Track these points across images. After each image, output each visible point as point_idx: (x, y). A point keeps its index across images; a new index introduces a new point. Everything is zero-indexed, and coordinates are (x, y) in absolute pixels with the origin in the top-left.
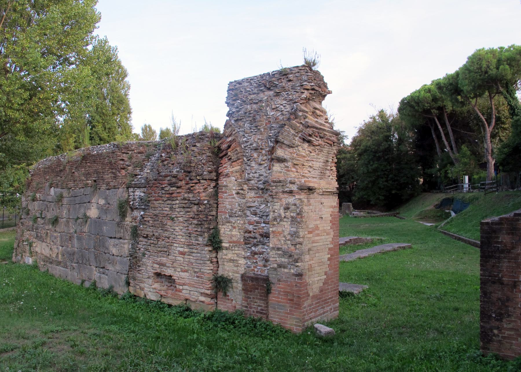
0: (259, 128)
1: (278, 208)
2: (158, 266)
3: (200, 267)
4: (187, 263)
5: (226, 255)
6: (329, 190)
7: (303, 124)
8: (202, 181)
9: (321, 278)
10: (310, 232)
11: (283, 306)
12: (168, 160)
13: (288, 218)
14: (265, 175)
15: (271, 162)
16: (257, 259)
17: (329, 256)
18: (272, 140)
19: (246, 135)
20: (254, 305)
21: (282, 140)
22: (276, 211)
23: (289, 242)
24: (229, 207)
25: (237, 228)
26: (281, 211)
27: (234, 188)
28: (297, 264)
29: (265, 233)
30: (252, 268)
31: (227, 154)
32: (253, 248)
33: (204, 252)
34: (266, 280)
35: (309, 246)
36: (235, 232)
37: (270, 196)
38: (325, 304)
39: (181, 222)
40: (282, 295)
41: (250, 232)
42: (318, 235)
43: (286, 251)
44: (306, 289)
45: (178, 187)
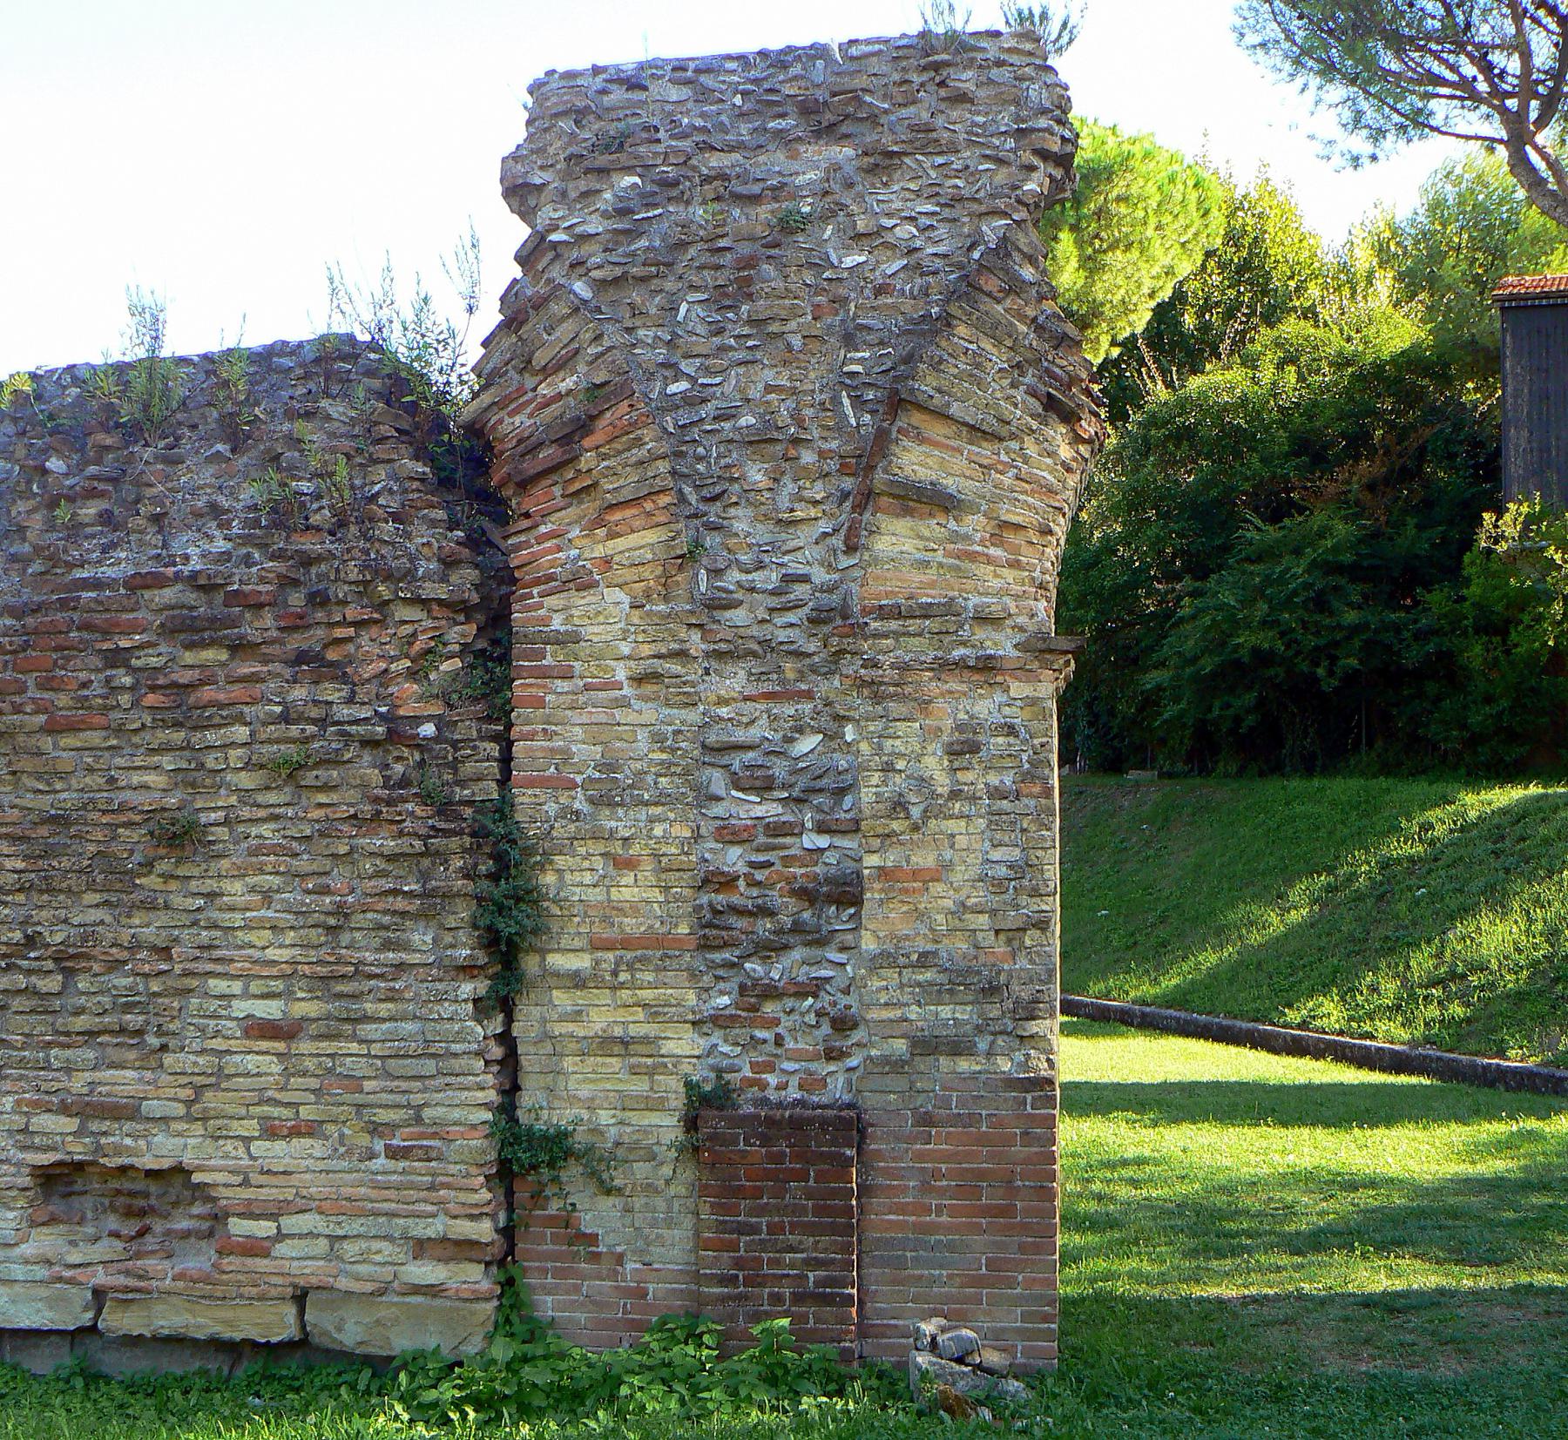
0: (774, 327)
2: (71, 1124)
3: (417, 1099)
4: (314, 1083)
5: (577, 1016)
8: (403, 612)
12: (102, 495)
13: (974, 799)
14: (820, 575)
15: (859, 508)
16: (777, 1022)
19: (687, 367)
20: (775, 1263)
21: (938, 400)
22: (901, 765)
23: (983, 920)
24: (586, 752)
25: (648, 865)
27: (625, 649)
29: (828, 880)
33: (447, 1009)
36: (628, 890)
37: (861, 683)
39: (275, 850)
40: (942, 1192)
41: (728, 882)
43: (963, 964)
45: (239, 648)
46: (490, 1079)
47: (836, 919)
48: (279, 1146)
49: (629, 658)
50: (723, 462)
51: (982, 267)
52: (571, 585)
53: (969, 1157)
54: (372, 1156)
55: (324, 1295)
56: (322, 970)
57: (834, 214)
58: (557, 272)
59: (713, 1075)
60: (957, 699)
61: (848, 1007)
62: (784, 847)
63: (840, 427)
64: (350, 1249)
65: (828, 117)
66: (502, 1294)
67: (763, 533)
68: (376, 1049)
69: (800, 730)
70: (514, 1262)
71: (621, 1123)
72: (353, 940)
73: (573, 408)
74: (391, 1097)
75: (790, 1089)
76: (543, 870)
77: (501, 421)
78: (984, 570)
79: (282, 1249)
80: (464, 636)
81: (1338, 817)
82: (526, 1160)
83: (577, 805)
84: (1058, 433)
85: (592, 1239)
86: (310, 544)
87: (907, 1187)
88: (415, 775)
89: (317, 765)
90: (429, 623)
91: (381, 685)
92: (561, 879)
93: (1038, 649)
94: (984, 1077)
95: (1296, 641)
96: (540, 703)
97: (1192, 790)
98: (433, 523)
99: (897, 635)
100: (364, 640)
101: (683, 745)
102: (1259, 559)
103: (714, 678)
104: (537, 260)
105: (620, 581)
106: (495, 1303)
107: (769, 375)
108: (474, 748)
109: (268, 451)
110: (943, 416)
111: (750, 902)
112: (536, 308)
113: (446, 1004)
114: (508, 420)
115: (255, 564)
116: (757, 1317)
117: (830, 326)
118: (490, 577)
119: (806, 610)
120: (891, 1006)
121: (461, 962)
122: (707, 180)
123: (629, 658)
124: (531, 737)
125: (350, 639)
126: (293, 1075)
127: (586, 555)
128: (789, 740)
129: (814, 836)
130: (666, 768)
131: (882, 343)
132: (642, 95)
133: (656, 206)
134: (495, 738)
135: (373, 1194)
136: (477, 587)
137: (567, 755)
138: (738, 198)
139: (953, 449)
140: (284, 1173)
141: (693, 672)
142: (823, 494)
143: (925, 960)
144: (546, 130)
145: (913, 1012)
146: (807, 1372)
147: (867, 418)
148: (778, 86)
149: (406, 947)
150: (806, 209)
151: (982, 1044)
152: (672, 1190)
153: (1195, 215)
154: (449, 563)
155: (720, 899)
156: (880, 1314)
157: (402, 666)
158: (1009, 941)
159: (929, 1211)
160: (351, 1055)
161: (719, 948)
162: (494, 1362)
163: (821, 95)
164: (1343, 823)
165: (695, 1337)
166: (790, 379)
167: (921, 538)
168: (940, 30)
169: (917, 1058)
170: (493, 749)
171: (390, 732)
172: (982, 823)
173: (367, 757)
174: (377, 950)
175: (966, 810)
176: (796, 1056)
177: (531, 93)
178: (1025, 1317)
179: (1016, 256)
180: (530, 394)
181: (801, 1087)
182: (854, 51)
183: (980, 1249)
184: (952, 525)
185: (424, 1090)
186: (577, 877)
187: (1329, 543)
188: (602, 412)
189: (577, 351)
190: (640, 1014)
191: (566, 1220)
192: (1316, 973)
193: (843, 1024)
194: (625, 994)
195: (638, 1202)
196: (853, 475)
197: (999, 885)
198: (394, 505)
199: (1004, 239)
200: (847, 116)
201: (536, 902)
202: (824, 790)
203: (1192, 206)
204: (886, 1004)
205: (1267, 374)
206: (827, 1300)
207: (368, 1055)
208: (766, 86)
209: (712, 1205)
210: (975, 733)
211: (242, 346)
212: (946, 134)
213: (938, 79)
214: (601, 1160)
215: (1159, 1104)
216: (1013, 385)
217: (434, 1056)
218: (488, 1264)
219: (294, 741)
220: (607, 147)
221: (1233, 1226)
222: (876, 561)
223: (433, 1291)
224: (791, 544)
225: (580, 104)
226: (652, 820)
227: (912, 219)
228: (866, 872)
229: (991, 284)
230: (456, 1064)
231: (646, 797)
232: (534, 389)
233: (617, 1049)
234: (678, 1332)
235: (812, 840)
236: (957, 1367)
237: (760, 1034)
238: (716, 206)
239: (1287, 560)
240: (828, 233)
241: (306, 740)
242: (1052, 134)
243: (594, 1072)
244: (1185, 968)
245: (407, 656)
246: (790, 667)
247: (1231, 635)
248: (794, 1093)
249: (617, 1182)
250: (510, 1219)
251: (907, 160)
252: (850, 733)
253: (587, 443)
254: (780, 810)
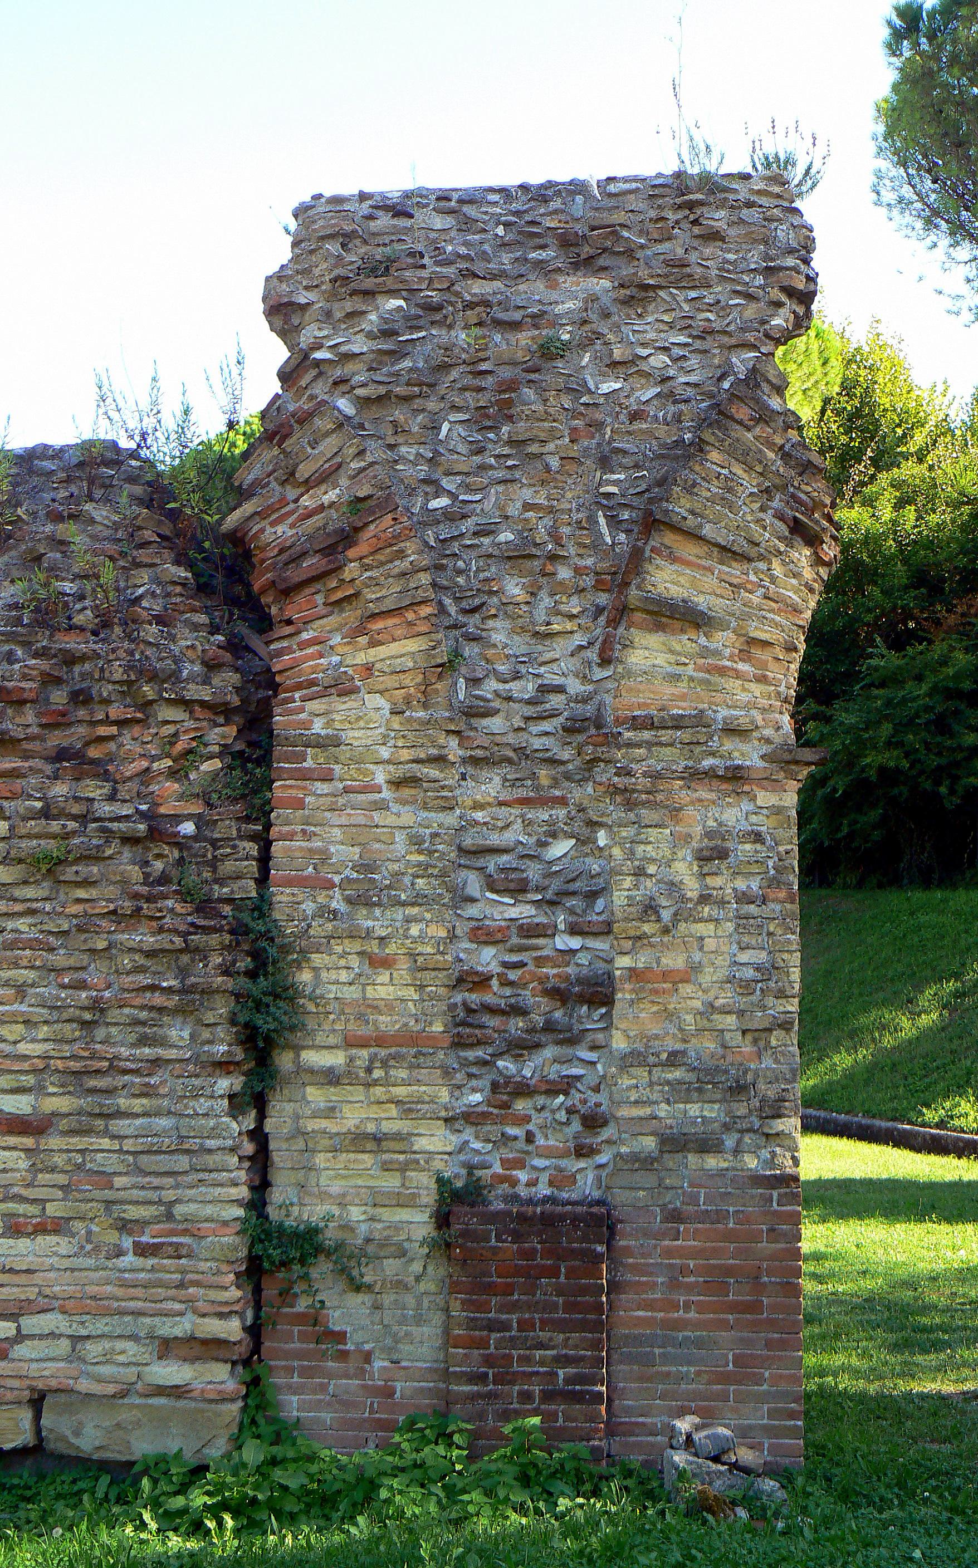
0: (534, 448)
3: (169, 1195)
4: (62, 1179)
5: (330, 1112)
11: (699, 1344)
13: (722, 903)
14: (575, 686)
15: (614, 622)
16: (527, 1119)
19: (448, 483)
21: (691, 522)
22: (651, 869)
23: (731, 1020)
24: (344, 854)
25: (404, 964)
26: (680, 867)
27: (385, 753)
29: (580, 981)
30: (498, 1168)
32: (506, 1064)
33: (203, 1105)
36: (384, 988)
37: (614, 791)
39: (32, 945)
40: (690, 1288)
41: (482, 982)
43: (711, 1063)
46: (242, 1175)
47: (587, 1017)
48: (23, 1244)
49: (388, 762)
50: (482, 576)
51: (733, 397)
52: (333, 690)
53: (715, 1253)
54: (120, 1253)
55: (62, 1398)
56: (74, 1065)
57: (591, 342)
58: (320, 390)
59: (464, 1172)
60: (706, 807)
61: (598, 1105)
62: (537, 948)
63: (596, 546)
64: (93, 1349)
65: (586, 250)
66: (246, 1396)
67: (519, 645)
68: (128, 1145)
69: (554, 835)
70: (260, 1360)
71: (372, 1219)
72: (109, 1035)
73: (336, 520)
74: (142, 1193)
75: (540, 1185)
76: (299, 968)
77: (262, 530)
78: (733, 684)
79: (21, 1350)
80: (224, 737)
81: (962, 927)
82: (276, 1257)
83: (334, 905)
84: (802, 555)
85: (341, 1337)
86: (72, 643)
87: (655, 1284)
88: (175, 873)
89: (77, 861)
90: (191, 724)
91: (142, 783)
92: (317, 977)
93: (782, 760)
94: (730, 1174)
95: (919, 761)
96: (299, 804)
97: (820, 900)
98: (196, 627)
99: (649, 745)
100: (126, 739)
101: (440, 847)
102: (882, 685)
103: (470, 783)
104: (300, 377)
105: (381, 687)
106: (240, 1404)
107: (527, 494)
108: (234, 847)
109: (31, 550)
110: (697, 537)
111: (503, 1001)
112: (301, 422)
113: (202, 1100)
114: (269, 530)
115: (18, 661)
116: (506, 1416)
117: (587, 449)
118: (248, 681)
119: (562, 719)
120: (642, 1105)
121: (218, 1058)
122: (470, 306)
123: (388, 762)
124: (290, 837)
125: (112, 738)
126: (41, 1171)
127: (348, 662)
128: (543, 844)
129: (566, 938)
130: (423, 870)
131: (637, 466)
132: (407, 223)
133: (419, 328)
134: (253, 838)
135: (120, 1292)
136: (238, 690)
137: (325, 856)
138: (498, 323)
139: (705, 568)
140: (28, 1271)
141: (450, 777)
142: (579, 609)
143: (675, 1059)
144: (312, 252)
145: (663, 1110)
146: (559, 1472)
147: (622, 537)
148: (538, 219)
149: (162, 1042)
150: (566, 337)
151: (730, 1142)
152: (422, 1287)
153: (818, 363)
154: (211, 666)
155: (474, 998)
156: (628, 1411)
157: (163, 764)
158: (755, 1041)
159: (676, 1307)
160: (103, 1151)
161: (471, 1046)
162: (244, 1465)
163: (580, 228)
164: (966, 932)
165: (445, 1437)
166: (548, 498)
167: (672, 652)
168: (695, 171)
169: (666, 1156)
170: (252, 848)
171: (151, 829)
172: (730, 926)
173: (127, 854)
174: (133, 1045)
175: (715, 913)
176: (547, 1153)
177: (296, 216)
178: (772, 1414)
179: (766, 387)
180: (292, 506)
181: (551, 1183)
182: (612, 188)
183: (727, 1347)
184: (703, 640)
185: (177, 1186)
186: (333, 975)
187: (951, 671)
188: (366, 525)
189: (340, 466)
190: (393, 1111)
191: (314, 1318)
192: (950, 1074)
193: (593, 1121)
194: (378, 1091)
195: (387, 1299)
196: (608, 591)
197: (746, 987)
198: (157, 608)
199: (754, 370)
200: (605, 250)
201: (292, 999)
202: (576, 894)
203: (815, 355)
204: (636, 1102)
205: (887, 513)
206: (577, 1398)
207: (120, 1151)
208: (528, 218)
209: (463, 1302)
210: (724, 839)
211: (7, 447)
212: (699, 270)
213: (692, 217)
214: (350, 1257)
215: (823, 1200)
216: (762, 509)
217: (187, 1152)
218: (234, 1363)
219: (54, 837)
220: (374, 270)
221: (925, 1320)
222: (629, 674)
223: (177, 1392)
224: (548, 656)
225: (348, 228)
226: (408, 920)
227: (666, 349)
228: (618, 973)
229: (742, 412)
230: (210, 1160)
231: (403, 897)
232: (296, 501)
233: (370, 1145)
234: (428, 1431)
235: (565, 941)
236: (714, 1467)
237: (512, 1131)
238: (476, 331)
239: (910, 685)
240: (586, 360)
241: (66, 836)
242: (798, 273)
243: (346, 1168)
244: (821, 1068)
245: (168, 756)
246: (544, 774)
247: (858, 757)
248: (544, 1190)
249: (367, 1279)
250: (257, 1317)
251: (661, 293)
252: (602, 838)
253: (351, 553)
254: (533, 912)
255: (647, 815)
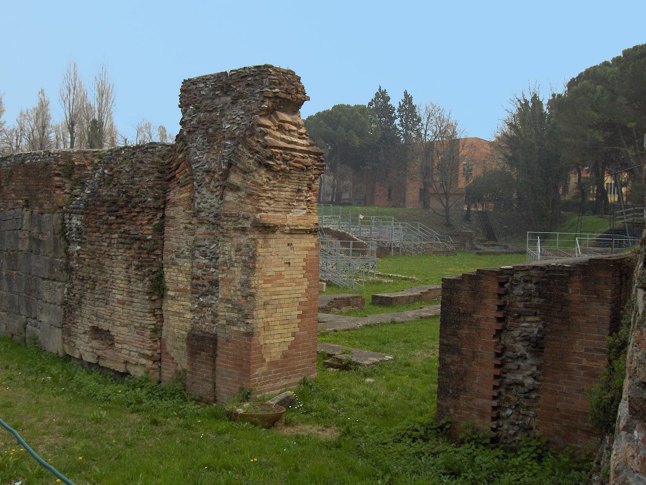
1: (228, 248)
4: (126, 315)
6: (300, 228)
7: (261, 144)
9: (285, 340)
10: (265, 282)
14: (217, 205)
17: (301, 312)
18: (226, 161)
22: (227, 253)
28: (248, 321)
31: (174, 176)
34: (214, 340)
35: (265, 299)
38: (290, 373)
41: (198, 278)
42: (282, 285)
44: (260, 353)
190: (182, 307)
233: (178, 315)
255: (226, 239)
